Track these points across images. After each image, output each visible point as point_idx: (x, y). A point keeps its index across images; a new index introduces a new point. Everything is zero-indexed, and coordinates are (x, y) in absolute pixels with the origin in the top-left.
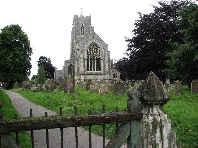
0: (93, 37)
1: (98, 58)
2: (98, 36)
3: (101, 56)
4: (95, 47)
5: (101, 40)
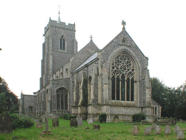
0: (124, 41)
1: (130, 78)
2: (132, 41)
3: (135, 75)
4: (125, 59)
5: (136, 48)
